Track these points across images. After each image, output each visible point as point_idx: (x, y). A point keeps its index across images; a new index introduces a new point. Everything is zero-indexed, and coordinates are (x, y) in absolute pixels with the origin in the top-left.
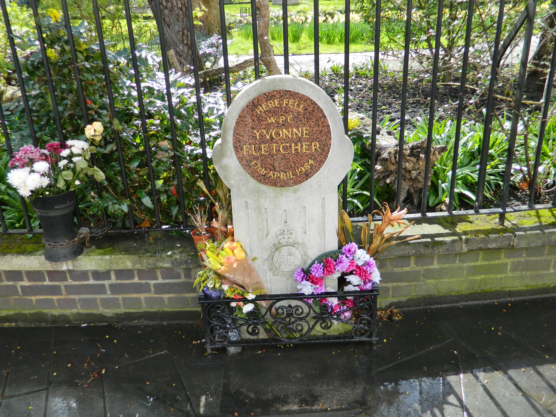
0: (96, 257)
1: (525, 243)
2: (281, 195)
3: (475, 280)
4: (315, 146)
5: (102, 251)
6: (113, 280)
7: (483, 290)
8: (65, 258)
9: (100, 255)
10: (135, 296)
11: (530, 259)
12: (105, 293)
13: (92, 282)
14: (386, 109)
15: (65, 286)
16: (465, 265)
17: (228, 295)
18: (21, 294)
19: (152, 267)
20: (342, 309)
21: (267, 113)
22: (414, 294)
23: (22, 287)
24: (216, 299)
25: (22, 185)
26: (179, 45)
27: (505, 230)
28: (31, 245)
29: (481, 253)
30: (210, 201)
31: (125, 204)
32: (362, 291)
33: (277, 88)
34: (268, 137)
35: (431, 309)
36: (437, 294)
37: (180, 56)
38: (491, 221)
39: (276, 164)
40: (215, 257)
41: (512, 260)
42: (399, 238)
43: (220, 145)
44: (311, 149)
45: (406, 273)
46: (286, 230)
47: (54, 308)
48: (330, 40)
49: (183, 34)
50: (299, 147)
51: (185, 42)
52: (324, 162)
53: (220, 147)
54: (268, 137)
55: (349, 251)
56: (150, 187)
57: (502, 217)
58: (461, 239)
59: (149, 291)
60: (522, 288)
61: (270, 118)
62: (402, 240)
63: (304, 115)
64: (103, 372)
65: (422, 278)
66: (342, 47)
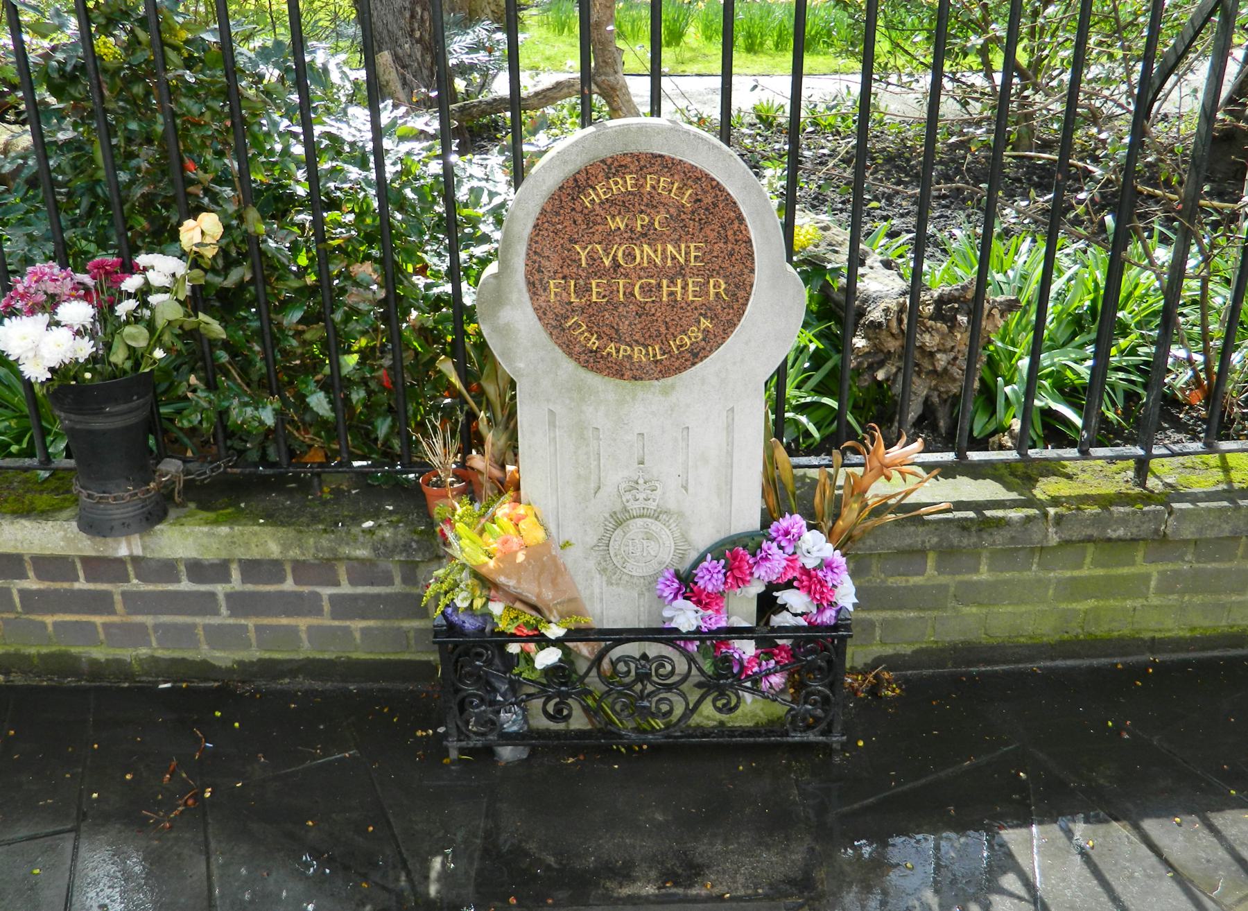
0: (197, 529)
2: (634, 399)
3: (1074, 610)
4: (716, 286)
5: (211, 515)
6: (236, 582)
8: (125, 529)
10: (284, 621)
11: (1201, 565)
12: (216, 613)
13: (185, 585)
14: (880, 208)
15: (124, 594)
17: (502, 626)
18: (19, 609)
19: (327, 555)
20: (764, 668)
21: (607, 206)
23: (24, 593)
24: (474, 635)
25: (31, 354)
26: (402, 40)
27: (1149, 498)
29: (1091, 548)
30: (466, 408)
31: (269, 408)
32: (812, 627)
33: (633, 149)
34: (607, 262)
36: (984, 639)
38: (1117, 477)
42: (901, 508)
44: (707, 293)
45: (917, 587)
46: (641, 481)
47: (96, 643)
49: (413, 16)
50: (679, 289)
51: (417, 34)
52: (735, 325)
54: (607, 262)
55: (787, 533)
57: (1142, 467)
58: (1046, 515)
59: (319, 612)
60: (1181, 634)
61: (613, 217)
62: (910, 514)
63: (693, 212)
64: (207, 795)
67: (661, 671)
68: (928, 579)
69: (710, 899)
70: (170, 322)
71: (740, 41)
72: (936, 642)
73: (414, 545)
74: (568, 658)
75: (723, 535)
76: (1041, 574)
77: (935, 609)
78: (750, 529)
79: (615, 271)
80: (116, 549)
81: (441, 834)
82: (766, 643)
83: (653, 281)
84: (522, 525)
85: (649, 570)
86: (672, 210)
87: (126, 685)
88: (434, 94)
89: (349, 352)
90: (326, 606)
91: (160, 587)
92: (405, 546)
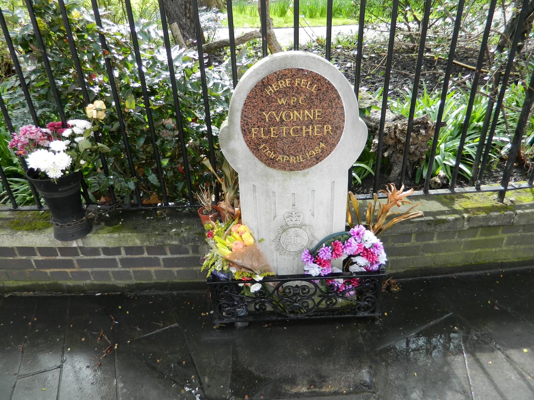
0: (105, 235)
1: (525, 220)
2: (290, 179)
5: (111, 228)
6: (123, 255)
7: (477, 262)
8: (73, 237)
9: (109, 233)
10: (145, 269)
11: (525, 234)
13: (102, 256)
14: (370, 79)
15: (77, 260)
16: (463, 240)
17: (237, 277)
18: (35, 267)
19: (160, 244)
20: (347, 288)
21: (277, 94)
22: (411, 266)
23: (36, 261)
26: (182, 18)
27: (505, 208)
28: (41, 222)
29: (480, 229)
30: (216, 181)
31: (132, 182)
32: (369, 272)
34: (278, 120)
35: (427, 280)
37: (183, 29)
38: (490, 197)
39: (286, 148)
40: (222, 241)
41: (508, 235)
43: (227, 127)
44: (323, 132)
45: (407, 247)
46: (294, 213)
49: (186, 8)
51: (188, 15)
52: (336, 145)
53: (227, 130)
54: (278, 120)
55: (358, 234)
56: (156, 165)
57: (502, 194)
59: (159, 265)
60: (514, 260)
61: (280, 99)
63: (317, 95)
64: (116, 347)
66: (325, 20)
68: (411, 244)
70: (86, 149)
72: (413, 267)
73: (197, 239)
74: (264, 288)
75: (329, 234)
76: (459, 240)
78: (341, 231)
79: (281, 123)
80: (72, 244)
81: (214, 364)
83: (298, 127)
85: (297, 249)
86: (307, 95)
87: (82, 294)
88: (195, 41)
91: (92, 257)
92: (193, 239)
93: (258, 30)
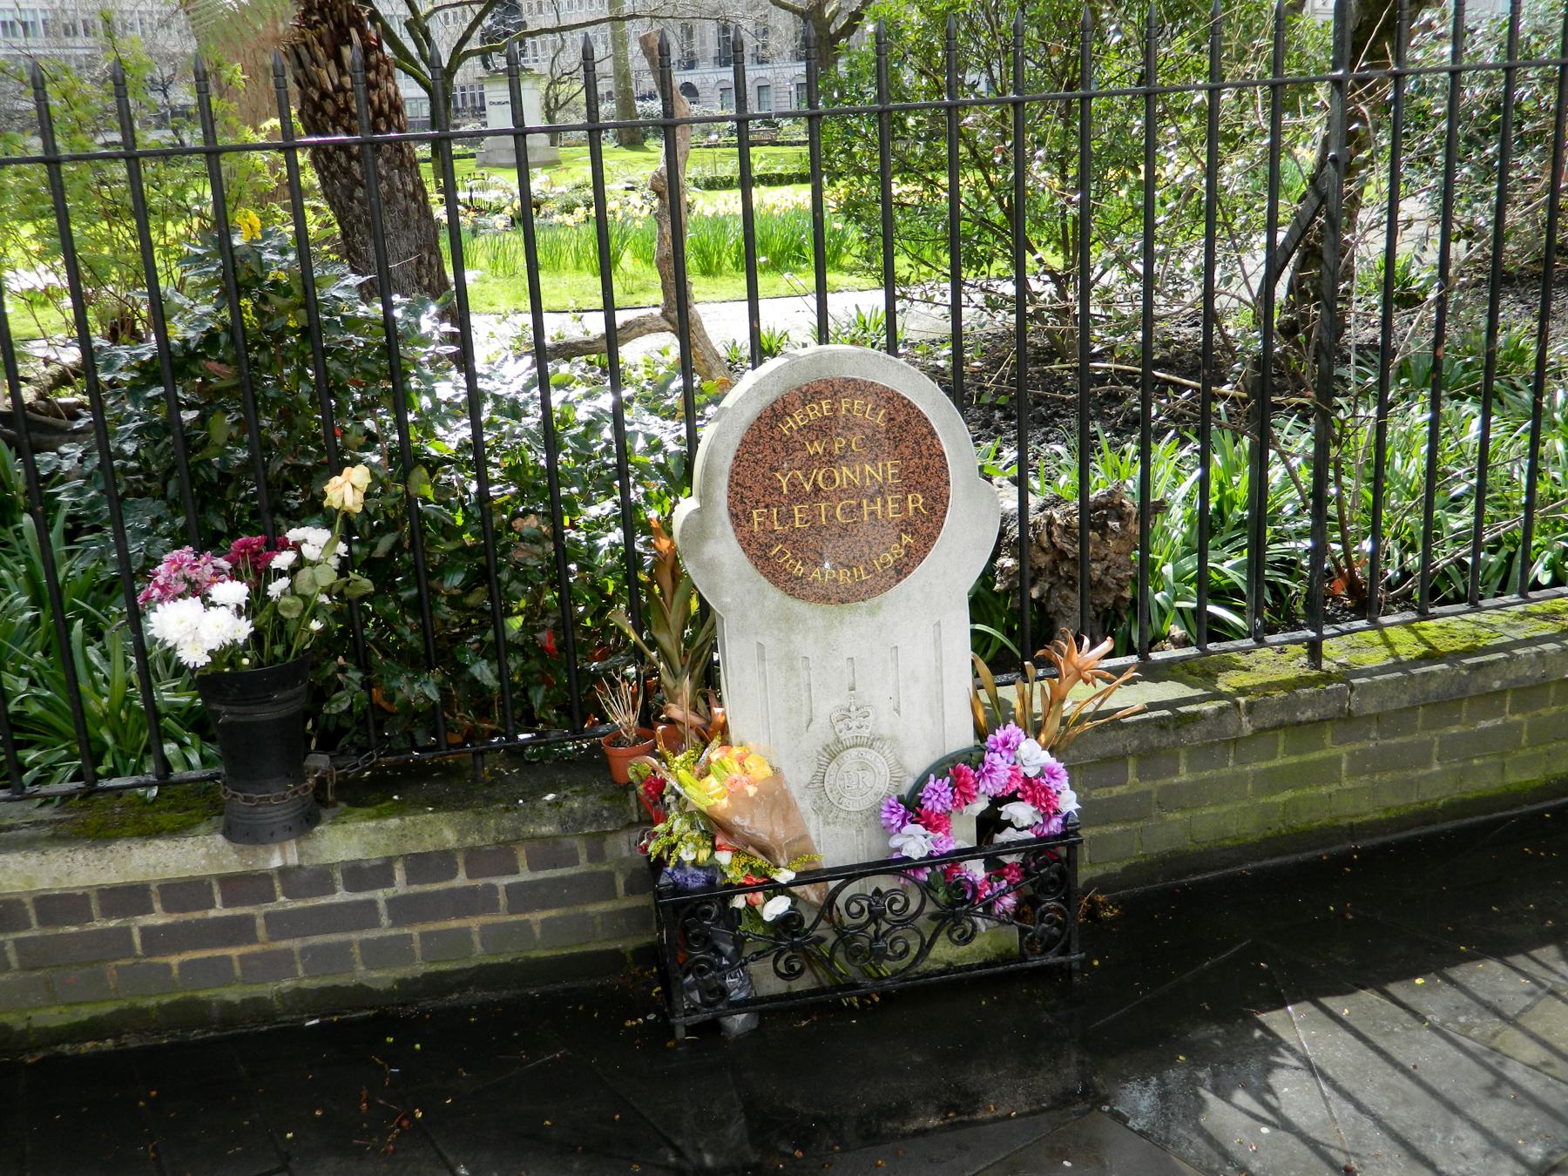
0: (362, 825)
1: (1374, 701)
2: (841, 622)
3: (1274, 804)
4: (915, 501)
10: (454, 924)
12: (375, 924)
13: (341, 896)
18: (139, 951)
19: (509, 837)
23: (146, 931)
24: (701, 889)
25: (190, 638)
27: (1328, 677)
33: (826, 375)
34: (808, 488)
36: (1191, 846)
41: (1348, 748)
42: (1097, 715)
44: (906, 509)
45: (1120, 798)
46: (853, 708)
47: (228, 980)
48: (709, 264)
50: (879, 507)
51: (426, 281)
54: (808, 488)
55: (1005, 743)
57: (1314, 650)
58: (1237, 704)
59: (493, 907)
60: (1377, 816)
61: (811, 442)
62: (1109, 722)
65: (1156, 811)
67: (896, 907)
69: (996, 1120)
71: (692, 263)
73: (605, 814)
75: (938, 756)
77: (1138, 819)
80: (267, 861)
82: (994, 866)
84: (747, 762)
89: (511, 615)
90: (502, 899)
93: (657, 312)
